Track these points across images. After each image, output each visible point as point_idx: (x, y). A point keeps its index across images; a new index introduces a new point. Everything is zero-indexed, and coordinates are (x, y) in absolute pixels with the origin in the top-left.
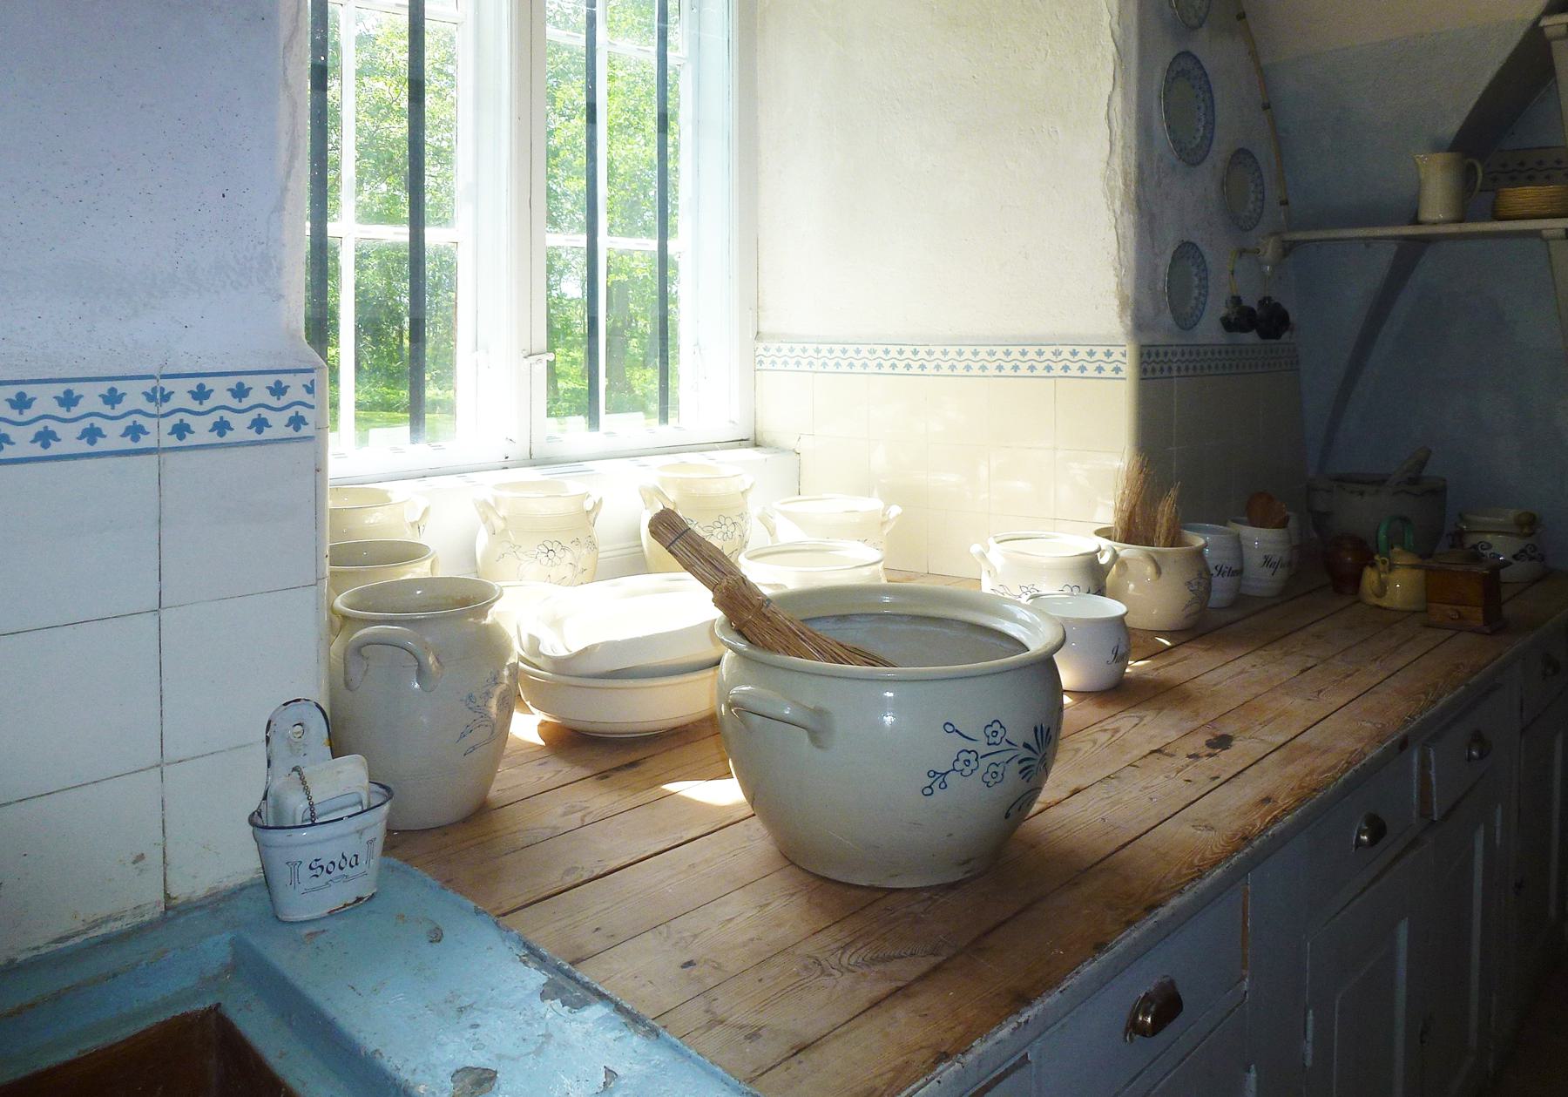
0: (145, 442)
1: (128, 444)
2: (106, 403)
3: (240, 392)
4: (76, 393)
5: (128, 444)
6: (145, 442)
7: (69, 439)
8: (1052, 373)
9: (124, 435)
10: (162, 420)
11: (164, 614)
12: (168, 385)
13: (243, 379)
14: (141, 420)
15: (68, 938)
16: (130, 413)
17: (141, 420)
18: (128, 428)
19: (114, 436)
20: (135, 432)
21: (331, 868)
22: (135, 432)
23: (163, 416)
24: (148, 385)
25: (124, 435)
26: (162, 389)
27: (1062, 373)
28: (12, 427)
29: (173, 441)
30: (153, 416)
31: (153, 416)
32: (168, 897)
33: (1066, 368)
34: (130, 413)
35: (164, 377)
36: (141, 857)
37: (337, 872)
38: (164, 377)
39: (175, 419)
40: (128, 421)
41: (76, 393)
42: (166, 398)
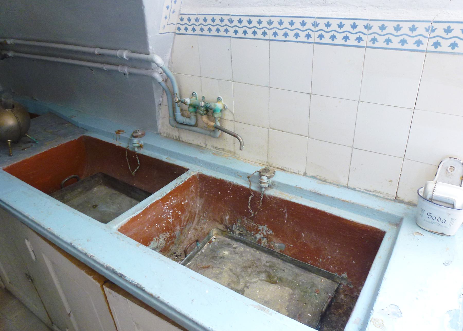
0: (421, 47)
1: (415, 47)
2: (301, 25)
3: (383, 28)
4: (400, 26)
5: (415, 47)
6: (421, 47)
7: (395, 43)
8: (362, 44)
9: (414, 44)
10: (430, 40)
11: (415, 110)
12: (435, 25)
13: (304, 19)
14: (421, 38)
15: (379, 192)
16: (271, 29)
17: (421, 38)
18: (331, 36)
19: (410, 44)
20: (419, 43)
21: (434, 218)
22: (419, 43)
23: (369, 35)
24: (427, 25)
25: (414, 44)
26: (433, 27)
27: (318, 40)
28: (410, 38)
29: (433, 49)
30: (427, 37)
31: (427, 37)
32: (397, 196)
33: (321, 37)
34: (271, 29)
35: (434, 22)
36: (391, 181)
37: (436, 221)
38: (434, 22)
39: (435, 40)
40: (417, 39)
41: (400, 26)
42: (433, 31)
